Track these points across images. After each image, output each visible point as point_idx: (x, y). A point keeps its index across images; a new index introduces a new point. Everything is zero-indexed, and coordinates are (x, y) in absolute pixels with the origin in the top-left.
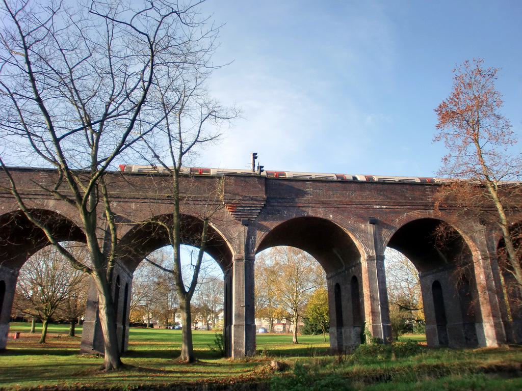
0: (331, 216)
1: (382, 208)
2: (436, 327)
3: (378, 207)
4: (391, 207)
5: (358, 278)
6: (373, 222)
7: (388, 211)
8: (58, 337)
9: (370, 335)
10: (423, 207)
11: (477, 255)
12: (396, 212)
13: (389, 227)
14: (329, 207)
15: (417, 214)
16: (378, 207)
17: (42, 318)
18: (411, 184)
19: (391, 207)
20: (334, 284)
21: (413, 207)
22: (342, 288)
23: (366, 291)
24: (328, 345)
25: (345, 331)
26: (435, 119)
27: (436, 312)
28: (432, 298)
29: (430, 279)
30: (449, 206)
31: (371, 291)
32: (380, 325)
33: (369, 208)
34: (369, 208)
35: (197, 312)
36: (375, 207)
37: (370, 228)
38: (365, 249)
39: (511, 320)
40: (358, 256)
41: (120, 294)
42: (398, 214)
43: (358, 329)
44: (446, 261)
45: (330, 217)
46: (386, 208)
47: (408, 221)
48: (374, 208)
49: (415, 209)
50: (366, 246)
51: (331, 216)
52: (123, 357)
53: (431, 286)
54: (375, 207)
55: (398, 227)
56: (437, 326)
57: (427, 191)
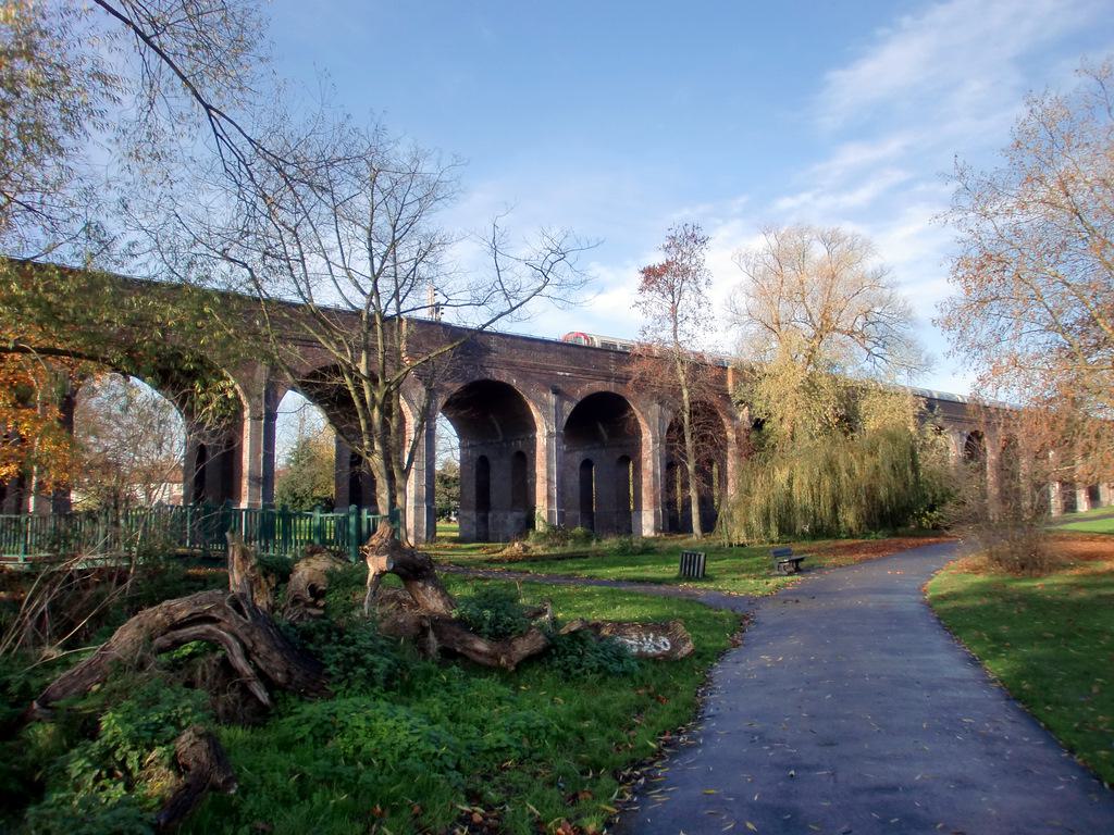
2: (579, 513)
5: (528, 456)
6: (556, 392)
8: (569, 577)
11: (647, 437)
13: (571, 399)
15: (599, 386)
17: (919, 589)
18: (552, 342)
20: (476, 456)
22: (493, 463)
23: (541, 470)
24: (457, 534)
25: (495, 516)
27: (581, 497)
28: (578, 479)
29: (577, 458)
30: (642, 385)
31: (549, 471)
35: (91, 466)
37: (552, 399)
40: (533, 429)
42: (580, 383)
43: (522, 515)
44: (606, 437)
50: (546, 415)
53: (579, 465)
55: (579, 400)
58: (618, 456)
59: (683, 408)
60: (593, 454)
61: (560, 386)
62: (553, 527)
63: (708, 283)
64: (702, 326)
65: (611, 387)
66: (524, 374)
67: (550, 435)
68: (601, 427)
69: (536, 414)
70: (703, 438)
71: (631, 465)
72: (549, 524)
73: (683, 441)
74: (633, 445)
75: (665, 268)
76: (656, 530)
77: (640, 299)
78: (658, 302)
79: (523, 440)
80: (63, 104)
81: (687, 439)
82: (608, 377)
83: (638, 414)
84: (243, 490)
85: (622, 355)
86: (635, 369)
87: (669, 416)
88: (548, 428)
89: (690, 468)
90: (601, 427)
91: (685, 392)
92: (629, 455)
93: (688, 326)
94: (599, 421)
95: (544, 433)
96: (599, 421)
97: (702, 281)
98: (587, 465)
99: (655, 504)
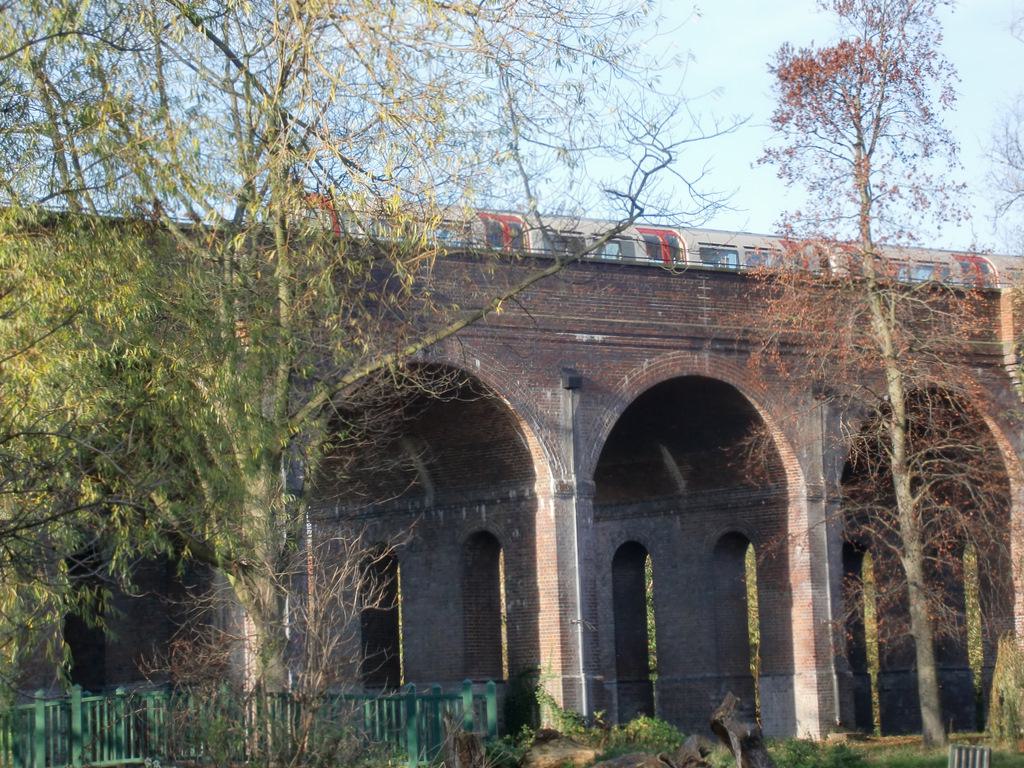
0: (478, 363)
1: (594, 343)
3: (585, 337)
4: (615, 339)
6: (575, 385)
7: (606, 350)
9: (554, 705)
10: (687, 343)
11: (797, 484)
12: (623, 356)
14: (472, 336)
16: (585, 337)
19: (615, 339)
21: (667, 342)
26: (767, 95)
29: (616, 531)
32: (580, 679)
33: (565, 342)
34: (565, 342)
36: (579, 337)
38: (552, 463)
39: (757, 641)
40: (526, 474)
41: (613, 650)
42: (629, 360)
44: (682, 484)
45: (474, 366)
46: (603, 343)
47: (652, 384)
48: (576, 342)
49: (669, 348)
50: (554, 452)
51: (478, 363)
52: (794, 730)
53: (609, 558)
54: (579, 337)
56: (619, 682)
57: (701, 292)
58: (715, 534)
59: (887, 410)
60: (644, 528)
61: (583, 369)
62: (578, 719)
63: (949, 96)
64: (934, 207)
65: (703, 363)
66: (507, 343)
67: (563, 492)
68: (669, 460)
69: (533, 442)
70: (943, 491)
71: (648, 560)
72: (569, 713)
73: (891, 501)
74: (521, 498)
75: (842, 57)
76: (826, 723)
77: (779, 142)
78: (827, 150)
79: (492, 502)
80: (318, 28)
81: (902, 490)
82: (695, 341)
83: (778, 437)
84: (750, 621)
85: (728, 281)
86: (774, 319)
87: (849, 432)
88: (556, 474)
89: (911, 566)
90: (669, 460)
91: (893, 374)
92: (758, 521)
93: (899, 209)
94: (679, 448)
95: (552, 482)
96: (679, 448)
97: (933, 88)
98: (630, 555)
99: (819, 656)
